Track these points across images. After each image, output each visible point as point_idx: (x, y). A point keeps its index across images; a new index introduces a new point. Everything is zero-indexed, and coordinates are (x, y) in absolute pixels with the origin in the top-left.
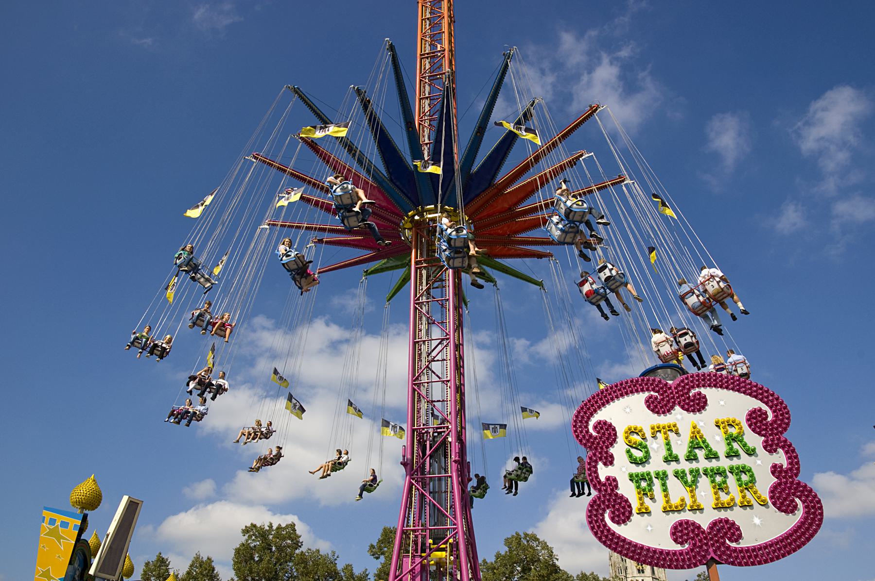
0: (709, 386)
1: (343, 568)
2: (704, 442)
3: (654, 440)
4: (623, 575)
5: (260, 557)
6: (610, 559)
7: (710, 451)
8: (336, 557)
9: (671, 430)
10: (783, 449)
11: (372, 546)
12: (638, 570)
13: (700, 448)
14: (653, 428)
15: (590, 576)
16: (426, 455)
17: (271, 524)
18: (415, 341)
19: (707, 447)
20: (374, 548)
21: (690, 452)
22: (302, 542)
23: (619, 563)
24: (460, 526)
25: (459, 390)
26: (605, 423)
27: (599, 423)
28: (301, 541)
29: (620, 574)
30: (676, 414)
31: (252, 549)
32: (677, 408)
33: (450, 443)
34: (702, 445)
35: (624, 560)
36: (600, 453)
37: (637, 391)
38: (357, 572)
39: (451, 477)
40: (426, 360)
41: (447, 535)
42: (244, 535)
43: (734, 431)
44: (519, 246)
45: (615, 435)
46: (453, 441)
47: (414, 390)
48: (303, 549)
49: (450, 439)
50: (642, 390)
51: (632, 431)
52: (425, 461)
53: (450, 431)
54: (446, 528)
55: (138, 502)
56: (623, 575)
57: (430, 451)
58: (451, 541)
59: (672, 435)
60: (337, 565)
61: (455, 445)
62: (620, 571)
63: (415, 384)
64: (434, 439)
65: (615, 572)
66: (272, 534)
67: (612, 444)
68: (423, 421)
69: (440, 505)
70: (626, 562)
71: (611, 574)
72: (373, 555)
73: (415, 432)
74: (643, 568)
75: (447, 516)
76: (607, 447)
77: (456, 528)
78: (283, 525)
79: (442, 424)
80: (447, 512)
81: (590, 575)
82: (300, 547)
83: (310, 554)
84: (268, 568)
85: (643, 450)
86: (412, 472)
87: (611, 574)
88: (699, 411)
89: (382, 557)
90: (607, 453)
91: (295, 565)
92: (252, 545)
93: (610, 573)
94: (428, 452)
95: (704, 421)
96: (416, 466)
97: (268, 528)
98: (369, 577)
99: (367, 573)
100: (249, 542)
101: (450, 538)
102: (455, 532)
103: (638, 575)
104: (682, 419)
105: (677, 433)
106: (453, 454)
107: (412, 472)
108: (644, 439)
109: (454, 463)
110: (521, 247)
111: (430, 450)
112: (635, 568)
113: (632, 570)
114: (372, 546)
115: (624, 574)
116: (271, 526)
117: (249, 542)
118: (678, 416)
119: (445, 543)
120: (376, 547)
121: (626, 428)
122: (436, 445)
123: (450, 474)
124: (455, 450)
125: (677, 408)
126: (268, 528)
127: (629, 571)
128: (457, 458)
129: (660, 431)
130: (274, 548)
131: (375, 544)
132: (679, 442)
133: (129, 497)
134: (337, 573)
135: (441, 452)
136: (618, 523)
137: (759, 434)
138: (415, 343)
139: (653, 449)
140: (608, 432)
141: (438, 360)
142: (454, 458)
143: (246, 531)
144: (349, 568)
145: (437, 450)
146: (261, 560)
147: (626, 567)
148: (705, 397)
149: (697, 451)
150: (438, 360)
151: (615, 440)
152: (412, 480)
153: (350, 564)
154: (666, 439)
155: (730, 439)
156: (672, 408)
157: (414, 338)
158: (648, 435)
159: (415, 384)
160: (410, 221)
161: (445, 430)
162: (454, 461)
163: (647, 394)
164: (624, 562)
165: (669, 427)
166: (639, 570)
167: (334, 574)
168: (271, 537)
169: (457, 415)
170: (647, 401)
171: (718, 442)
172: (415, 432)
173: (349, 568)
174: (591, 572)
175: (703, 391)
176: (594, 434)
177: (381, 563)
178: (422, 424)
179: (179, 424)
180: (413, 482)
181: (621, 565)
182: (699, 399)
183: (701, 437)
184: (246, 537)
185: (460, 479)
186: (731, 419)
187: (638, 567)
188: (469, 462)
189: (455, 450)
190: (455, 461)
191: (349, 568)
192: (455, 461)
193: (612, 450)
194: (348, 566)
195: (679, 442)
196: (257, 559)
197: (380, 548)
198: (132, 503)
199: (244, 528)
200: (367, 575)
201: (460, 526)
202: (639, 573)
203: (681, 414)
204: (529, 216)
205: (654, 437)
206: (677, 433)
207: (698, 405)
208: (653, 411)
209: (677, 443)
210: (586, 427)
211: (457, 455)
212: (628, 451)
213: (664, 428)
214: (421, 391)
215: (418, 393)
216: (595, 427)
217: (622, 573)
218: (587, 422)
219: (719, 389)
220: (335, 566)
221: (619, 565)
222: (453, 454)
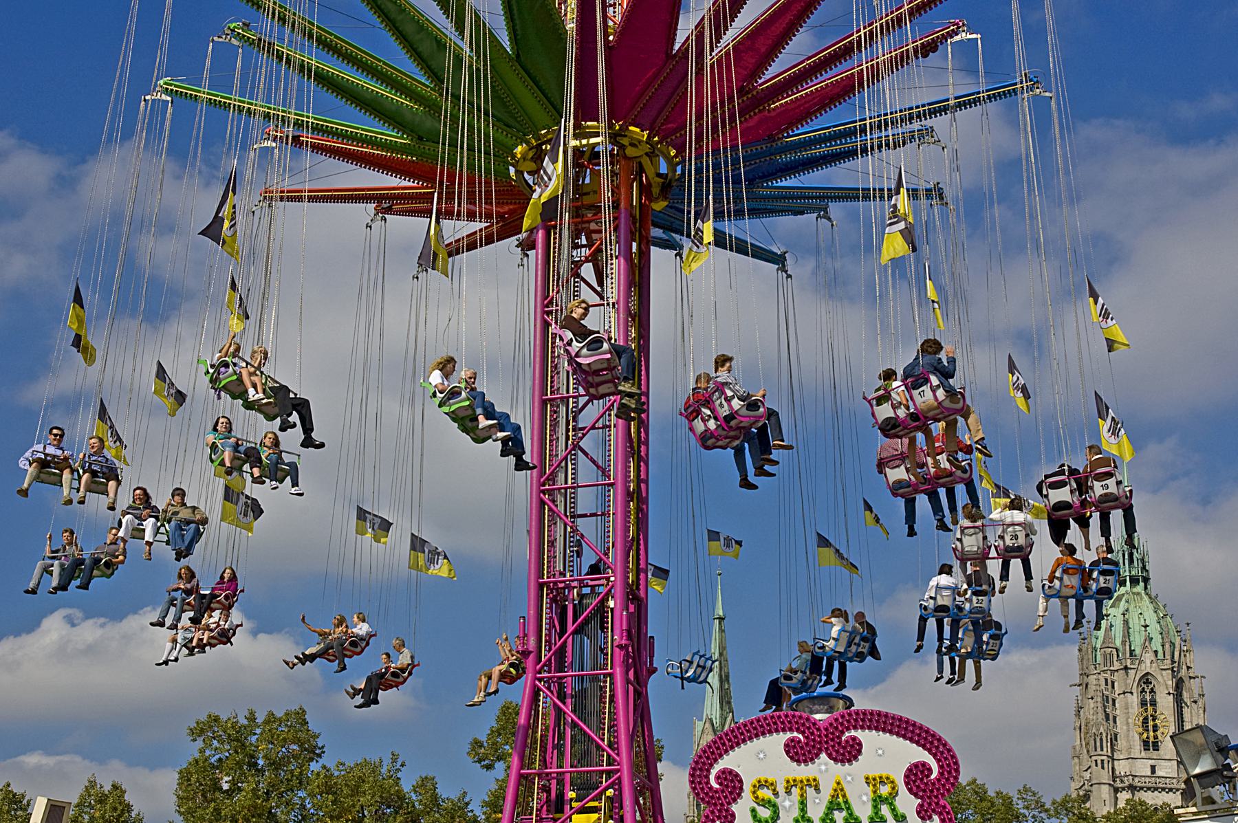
0: (870, 728)
1: (415, 784)
2: (846, 802)
3: (787, 797)
4: (1104, 752)
5: (233, 783)
6: (1078, 714)
7: (851, 814)
8: (398, 767)
9: (810, 786)
10: (939, 817)
11: (477, 744)
12: (1144, 741)
13: (840, 810)
14: (788, 782)
15: (967, 788)
16: (566, 632)
17: (252, 713)
18: (544, 397)
19: (848, 809)
20: (481, 746)
21: (827, 815)
22: (323, 747)
23: (1098, 725)
24: (625, 767)
25: (638, 497)
26: (731, 772)
27: (724, 771)
28: (320, 745)
29: (1099, 752)
30: (820, 765)
31: (213, 767)
32: (823, 756)
33: (612, 609)
34: (843, 807)
35: (1111, 718)
36: (720, 811)
37: (777, 731)
38: (448, 792)
39: (610, 675)
40: (571, 427)
41: (601, 782)
42: (195, 740)
43: (885, 790)
44: (780, 184)
45: (741, 789)
46: (618, 606)
47: (542, 503)
48: (329, 760)
49: (611, 604)
50: (784, 730)
51: (761, 785)
52: (565, 642)
53: (613, 586)
54: (600, 771)
55: (64, 805)
56: (1104, 752)
57: (573, 624)
58: (610, 792)
59: (810, 791)
60: (402, 782)
61: (622, 615)
62: (1098, 744)
63: (544, 492)
64: (580, 602)
65: (1087, 744)
66: (255, 734)
67: (735, 800)
68: (559, 567)
69: (591, 730)
70: (1115, 722)
71: (1078, 748)
72: (479, 761)
73: (545, 589)
74: (1156, 737)
75: (604, 750)
76: (729, 803)
77: (618, 771)
78: (279, 714)
79: (577, 620)
80: (603, 740)
81: (968, 785)
82: (319, 756)
83: (343, 773)
84: (255, 806)
85: (771, 808)
86: (538, 667)
87: (1078, 748)
88: (849, 761)
89: (500, 766)
90: (727, 810)
91: (312, 795)
92: (213, 760)
93: (1074, 748)
94: (571, 628)
95: (853, 776)
96: (545, 655)
97: (245, 722)
98: (470, 807)
99: (467, 800)
100: (208, 753)
101: (607, 788)
102: (609, 781)
103: (1143, 754)
104: (827, 770)
105: (817, 790)
106: (617, 631)
107: (538, 667)
108: (776, 794)
109: (618, 650)
110: (784, 183)
111: (574, 623)
112: (1137, 737)
113: (1128, 741)
114: (477, 744)
115: (1107, 750)
116: (252, 718)
117: (208, 753)
118: (824, 768)
119: (598, 798)
120: (486, 745)
121: (755, 781)
122: (585, 614)
123: (609, 671)
124: (621, 626)
125: (823, 756)
126: (245, 722)
127: (1121, 743)
128: (624, 642)
129: (796, 786)
130: (261, 762)
131: (484, 739)
132: (817, 801)
133: (49, 799)
134: (401, 797)
135: (595, 623)
136: (924, 764)
137: (916, 795)
138: (544, 403)
139: (785, 807)
140: (732, 782)
141: (599, 428)
142: (618, 640)
143: (198, 731)
144: (429, 786)
145: (587, 622)
146: (235, 789)
147: (1116, 735)
148: (860, 744)
149: (836, 813)
150: (599, 428)
151: (739, 795)
152: (537, 682)
153: (431, 775)
154: (802, 796)
155: (878, 801)
156: (817, 755)
157: (543, 391)
158: (781, 789)
159: (544, 492)
160: (532, 158)
161: (604, 581)
162: (617, 646)
163: (789, 735)
164: (1111, 722)
165: (808, 780)
166: (1146, 743)
167: (397, 801)
168: (254, 738)
169: (630, 548)
170: (786, 745)
171: (864, 803)
172: (545, 589)
173: (426, 784)
174: (971, 780)
175: (858, 734)
176: (716, 786)
177: (497, 780)
178: (557, 574)
179: (67, 590)
180: (540, 685)
181: (1102, 730)
182: (852, 746)
183: (844, 796)
184: (200, 743)
185: (631, 673)
186: (884, 775)
187: (1145, 735)
188: (652, 638)
189: (621, 626)
190: (620, 647)
191: (426, 784)
192: (620, 647)
193: (734, 808)
194: (425, 780)
195: (817, 801)
196: (226, 787)
197: (495, 746)
198: (53, 808)
199: (193, 725)
200: (467, 804)
201: (625, 767)
202: (1147, 749)
203: (826, 764)
204: (815, 81)
205: (788, 792)
206: (817, 790)
207: (849, 753)
208: (792, 758)
209: (815, 802)
210: (707, 777)
211: (624, 634)
212: (753, 810)
213: (802, 781)
214: (556, 506)
215: (550, 509)
216: (717, 778)
217: (1102, 750)
218: (709, 771)
219: (881, 733)
220: (397, 784)
221: (1098, 730)
222: (617, 631)
